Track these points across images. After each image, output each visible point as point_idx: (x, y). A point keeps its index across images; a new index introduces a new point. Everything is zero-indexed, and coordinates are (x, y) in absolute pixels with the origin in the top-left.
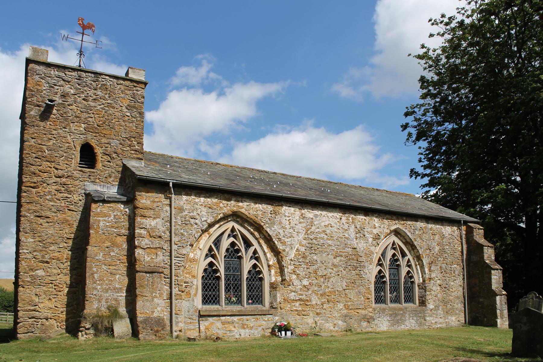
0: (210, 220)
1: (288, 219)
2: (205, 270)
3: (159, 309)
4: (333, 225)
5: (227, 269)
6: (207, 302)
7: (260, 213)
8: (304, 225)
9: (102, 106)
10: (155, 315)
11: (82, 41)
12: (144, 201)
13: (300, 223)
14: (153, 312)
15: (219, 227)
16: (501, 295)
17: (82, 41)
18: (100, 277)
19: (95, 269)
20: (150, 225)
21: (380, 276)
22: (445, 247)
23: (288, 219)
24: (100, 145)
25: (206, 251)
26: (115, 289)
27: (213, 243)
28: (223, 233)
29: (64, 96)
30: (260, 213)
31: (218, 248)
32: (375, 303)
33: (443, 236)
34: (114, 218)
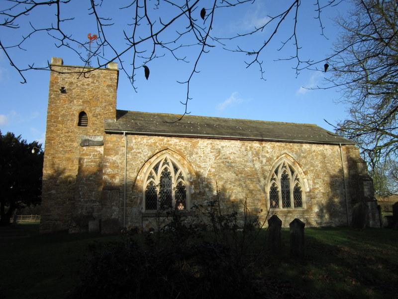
0: (150, 154)
1: (203, 150)
2: (148, 186)
3: (115, 213)
4: (235, 152)
5: (282, 187)
6: (149, 208)
7: (183, 148)
8: (214, 154)
9: (92, 88)
10: (113, 217)
11: (118, 56)
12: (109, 145)
13: (211, 152)
14: (112, 215)
15: (156, 158)
16: (372, 201)
17: (118, 56)
18: (83, 193)
19: (80, 189)
20: (112, 160)
21: (274, 190)
22: (327, 164)
23: (203, 150)
24: (91, 111)
25: (148, 174)
26: (91, 201)
27: (153, 169)
28: (160, 161)
29: (71, 83)
30: (183, 148)
31: (157, 173)
32: (295, 207)
33: (324, 156)
34: (93, 156)
